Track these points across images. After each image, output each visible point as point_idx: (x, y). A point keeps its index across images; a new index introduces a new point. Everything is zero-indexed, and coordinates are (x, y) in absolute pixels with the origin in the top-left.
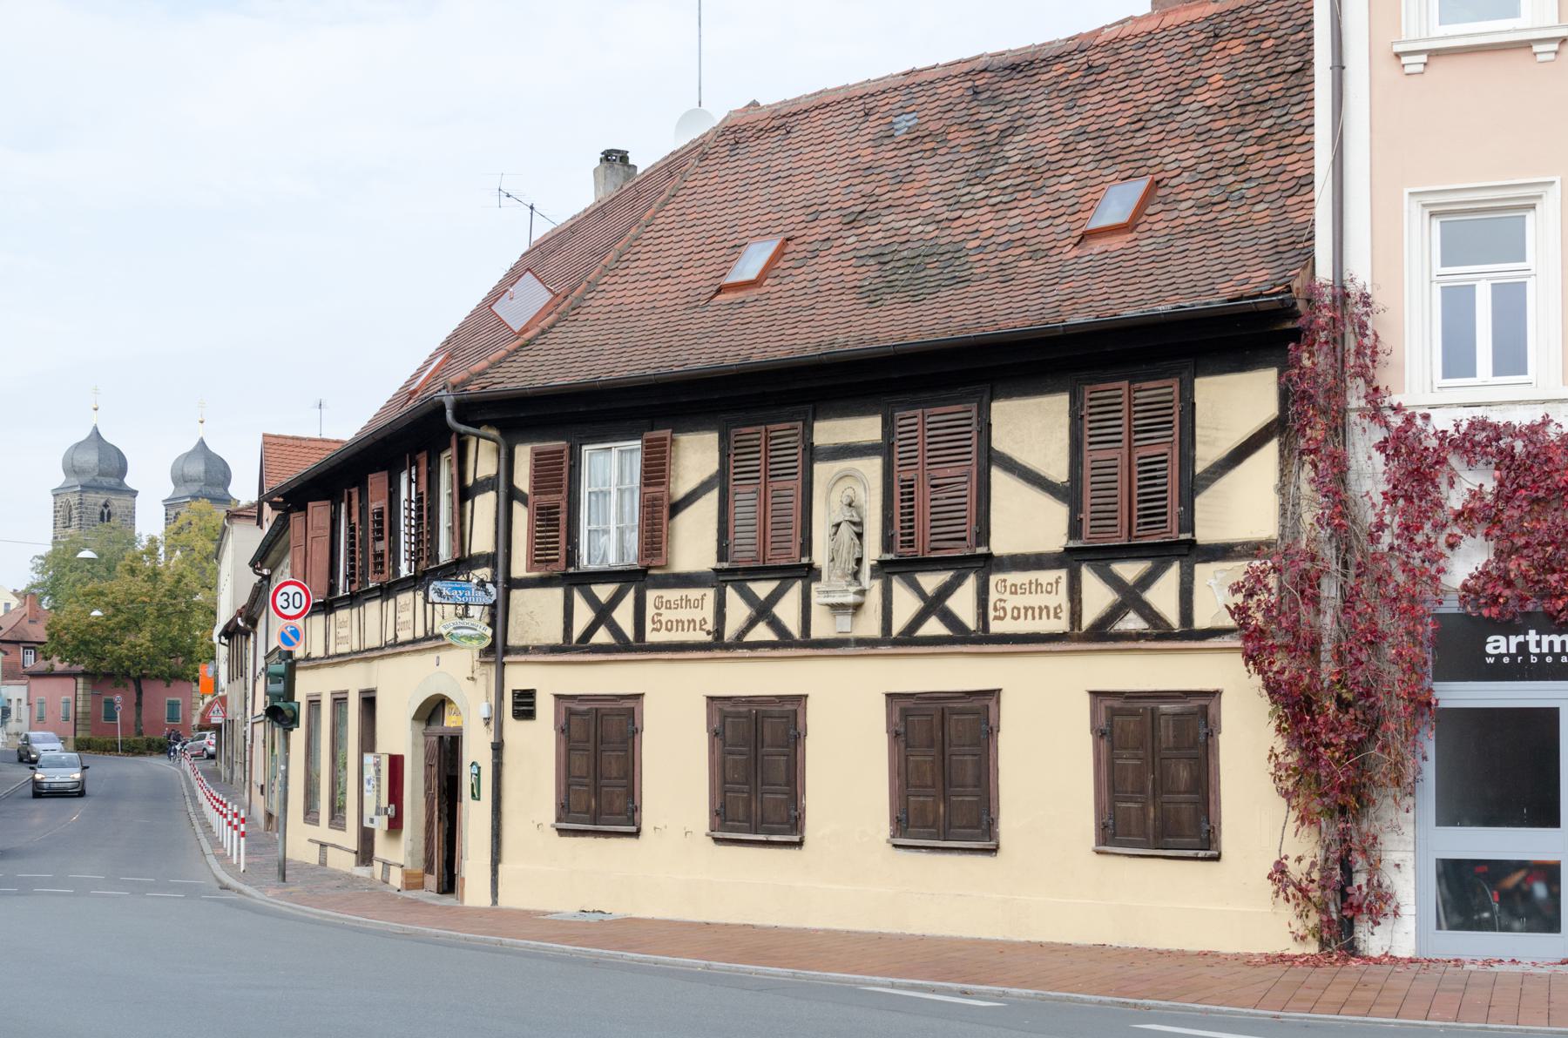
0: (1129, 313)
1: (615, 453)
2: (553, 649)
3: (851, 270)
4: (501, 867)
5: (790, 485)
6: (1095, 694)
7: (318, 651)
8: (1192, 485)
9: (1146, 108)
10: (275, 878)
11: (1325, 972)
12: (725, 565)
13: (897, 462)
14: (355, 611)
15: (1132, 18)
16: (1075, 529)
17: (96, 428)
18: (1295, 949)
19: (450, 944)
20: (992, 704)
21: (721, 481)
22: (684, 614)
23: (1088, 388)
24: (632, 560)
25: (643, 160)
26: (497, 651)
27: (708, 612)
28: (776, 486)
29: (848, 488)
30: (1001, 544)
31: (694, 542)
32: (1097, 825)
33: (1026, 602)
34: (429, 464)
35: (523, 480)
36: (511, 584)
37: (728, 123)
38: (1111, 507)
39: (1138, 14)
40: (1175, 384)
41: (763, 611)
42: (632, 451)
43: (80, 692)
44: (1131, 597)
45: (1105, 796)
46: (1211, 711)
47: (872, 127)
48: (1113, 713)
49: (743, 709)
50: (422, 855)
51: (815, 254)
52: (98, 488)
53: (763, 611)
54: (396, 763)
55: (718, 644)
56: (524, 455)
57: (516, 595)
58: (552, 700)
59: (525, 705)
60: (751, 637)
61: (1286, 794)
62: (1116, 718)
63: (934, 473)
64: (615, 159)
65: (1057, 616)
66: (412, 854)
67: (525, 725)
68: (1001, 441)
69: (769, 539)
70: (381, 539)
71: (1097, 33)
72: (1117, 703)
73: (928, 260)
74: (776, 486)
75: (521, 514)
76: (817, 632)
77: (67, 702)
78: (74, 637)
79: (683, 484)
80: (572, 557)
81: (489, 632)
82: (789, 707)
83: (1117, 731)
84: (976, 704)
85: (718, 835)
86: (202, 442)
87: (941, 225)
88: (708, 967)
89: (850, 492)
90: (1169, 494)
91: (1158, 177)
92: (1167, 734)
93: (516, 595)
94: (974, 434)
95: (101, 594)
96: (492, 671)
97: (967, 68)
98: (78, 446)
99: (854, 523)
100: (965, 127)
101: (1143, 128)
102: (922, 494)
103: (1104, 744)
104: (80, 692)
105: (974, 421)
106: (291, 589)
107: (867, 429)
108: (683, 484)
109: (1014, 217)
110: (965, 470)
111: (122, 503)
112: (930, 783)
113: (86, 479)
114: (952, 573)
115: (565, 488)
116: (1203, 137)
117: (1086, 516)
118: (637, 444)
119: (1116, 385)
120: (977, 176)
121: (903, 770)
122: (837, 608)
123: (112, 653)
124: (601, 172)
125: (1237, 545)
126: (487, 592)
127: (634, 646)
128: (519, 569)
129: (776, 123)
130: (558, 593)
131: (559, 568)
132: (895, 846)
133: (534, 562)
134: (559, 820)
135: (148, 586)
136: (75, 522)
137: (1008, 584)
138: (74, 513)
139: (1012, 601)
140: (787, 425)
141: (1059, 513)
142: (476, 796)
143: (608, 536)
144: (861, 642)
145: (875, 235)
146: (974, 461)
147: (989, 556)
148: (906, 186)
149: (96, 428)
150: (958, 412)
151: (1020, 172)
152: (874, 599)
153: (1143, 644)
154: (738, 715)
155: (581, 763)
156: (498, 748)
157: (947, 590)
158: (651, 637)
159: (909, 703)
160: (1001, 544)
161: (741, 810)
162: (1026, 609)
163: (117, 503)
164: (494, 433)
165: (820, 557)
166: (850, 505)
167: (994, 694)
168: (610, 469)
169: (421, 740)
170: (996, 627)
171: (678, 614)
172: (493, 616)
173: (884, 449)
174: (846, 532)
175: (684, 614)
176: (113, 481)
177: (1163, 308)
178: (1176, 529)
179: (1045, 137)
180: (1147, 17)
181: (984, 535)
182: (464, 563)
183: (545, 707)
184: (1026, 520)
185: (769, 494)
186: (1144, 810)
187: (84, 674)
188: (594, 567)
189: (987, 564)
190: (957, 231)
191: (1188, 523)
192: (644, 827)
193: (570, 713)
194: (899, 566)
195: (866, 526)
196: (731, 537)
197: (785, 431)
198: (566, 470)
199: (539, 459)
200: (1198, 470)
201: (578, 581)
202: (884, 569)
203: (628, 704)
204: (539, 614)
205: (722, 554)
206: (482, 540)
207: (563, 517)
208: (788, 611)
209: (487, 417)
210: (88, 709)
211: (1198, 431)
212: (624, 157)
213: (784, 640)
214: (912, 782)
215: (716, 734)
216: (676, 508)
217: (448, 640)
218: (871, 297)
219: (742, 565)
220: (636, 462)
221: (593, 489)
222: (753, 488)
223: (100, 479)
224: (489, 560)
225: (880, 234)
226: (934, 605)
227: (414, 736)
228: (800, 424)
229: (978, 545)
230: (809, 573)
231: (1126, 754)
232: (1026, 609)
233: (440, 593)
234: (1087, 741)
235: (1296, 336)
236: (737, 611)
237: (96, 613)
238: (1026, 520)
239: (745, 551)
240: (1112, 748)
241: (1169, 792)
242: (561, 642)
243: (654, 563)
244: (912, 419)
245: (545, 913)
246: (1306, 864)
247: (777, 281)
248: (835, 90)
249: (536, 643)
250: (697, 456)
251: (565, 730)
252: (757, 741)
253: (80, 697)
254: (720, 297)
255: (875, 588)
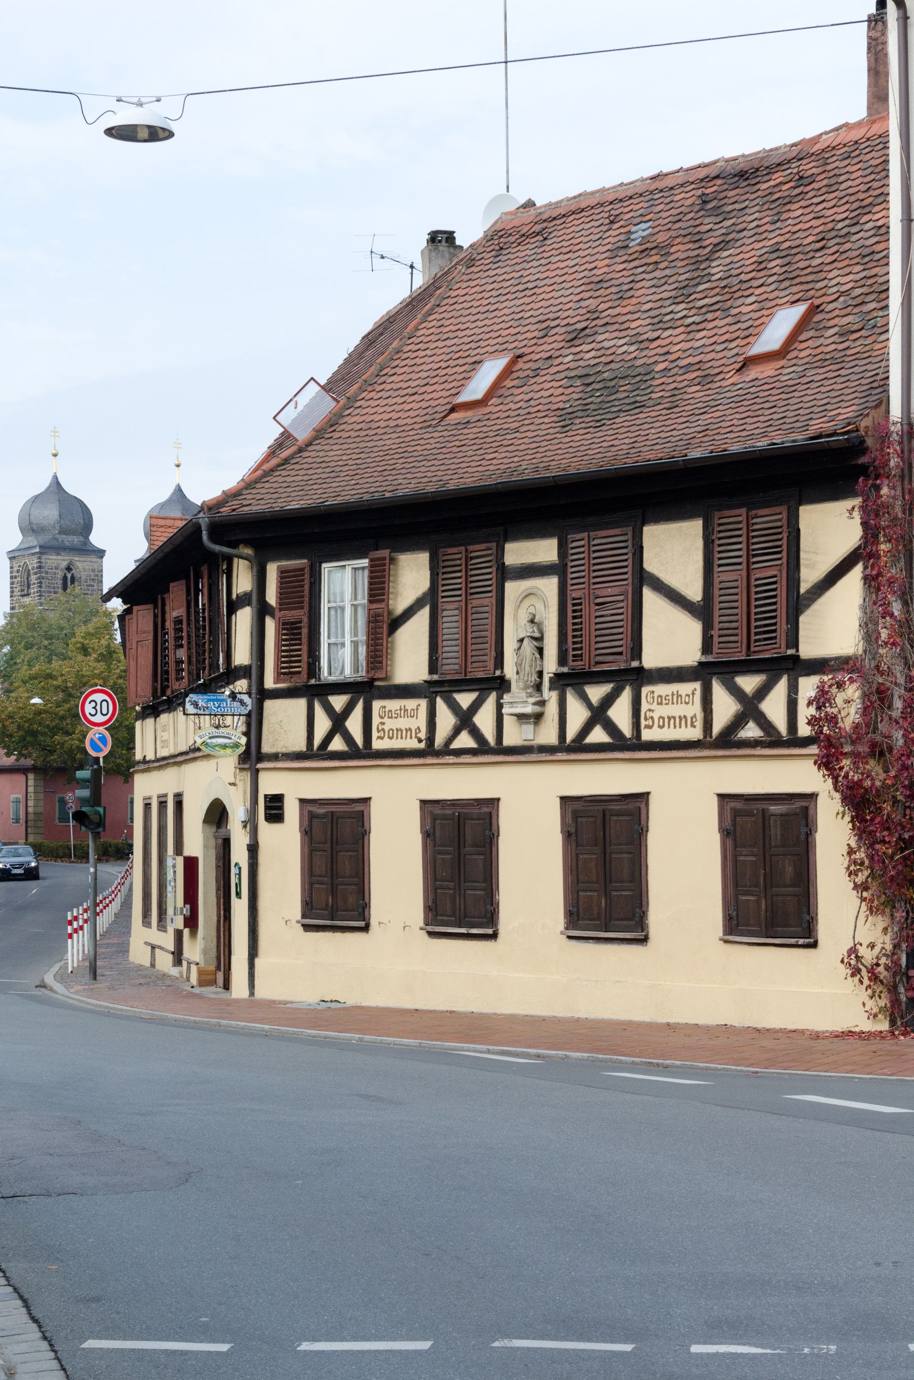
0: (735, 448)
1: (349, 570)
2: (298, 756)
3: (560, 390)
4: (257, 961)
5: (486, 601)
6: (722, 797)
7: (150, 756)
8: (798, 604)
9: (830, 226)
10: (87, 977)
11: (888, 1044)
12: (435, 677)
13: (570, 582)
14: (171, 714)
15: (846, 125)
16: (707, 647)
17: (55, 478)
18: (867, 1026)
19: (109, 1014)
20: (643, 806)
21: (431, 598)
22: (403, 723)
23: (717, 514)
24: (362, 674)
25: (468, 236)
26: (253, 757)
27: (421, 721)
28: (475, 603)
29: (531, 608)
30: (651, 659)
31: (410, 660)
32: (425, 907)
33: (672, 711)
34: (210, 577)
35: (272, 598)
36: (262, 695)
37: (498, 227)
38: (734, 625)
39: (852, 120)
40: (783, 509)
41: (465, 720)
42: (363, 568)
43: (31, 789)
44: (750, 709)
45: (730, 891)
46: (811, 812)
47: (613, 236)
48: (736, 813)
49: (448, 812)
50: (213, 953)
51: (536, 373)
52: (58, 549)
53: (465, 720)
54: (191, 864)
55: (431, 752)
56: (272, 571)
57: (269, 704)
58: (297, 803)
59: (275, 809)
60: (456, 745)
61: (861, 887)
62: (738, 819)
63: (598, 592)
64: (441, 240)
65: (693, 726)
66: (205, 952)
67: (275, 827)
68: (651, 564)
69: (469, 654)
70: (181, 646)
71: (816, 140)
72: (739, 805)
73: (622, 382)
74: (475, 603)
75: (270, 625)
76: (508, 741)
77: (17, 801)
78: (19, 727)
79: (401, 602)
80: (313, 668)
81: (244, 740)
82: (485, 810)
83: (739, 830)
84: (631, 806)
85: (430, 928)
86: (179, 490)
87: (643, 346)
88: (360, 1040)
89: (532, 610)
90: (778, 613)
91: (817, 302)
92: (776, 832)
93: (269, 704)
94: (630, 555)
95: (50, 676)
96: (247, 776)
97: (702, 173)
98: (36, 499)
99: (536, 639)
100: (687, 239)
101: (823, 248)
102: (589, 612)
103: (729, 842)
104: (31, 789)
105: (630, 543)
106: (98, 697)
107: (544, 550)
108: (401, 602)
109: (701, 339)
110: (623, 589)
111: (87, 565)
112: (594, 879)
113: (45, 539)
114: (612, 685)
115: (306, 605)
116: (867, 259)
117: (715, 633)
118: (365, 562)
119: (737, 511)
120: (683, 294)
121: (574, 867)
122: (521, 717)
123: (62, 745)
124: (427, 252)
125: (830, 659)
126: (242, 702)
127: (362, 754)
128: (269, 682)
129: (537, 228)
130: (301, 704)
131: (300, 680)
132: (569, 937)
133: (279, 677)
134: (304, 916)
135: (101, 666)
136: (34, 589)
137: (656, 695)
138: (33, 578)
139: (661, 711)
140: (483, 546)
141: (693, 629)
142: (238, 895)
143: (341, 652)
144: (543, 749)
145: (588, 353)
146: (630, 581)
147: (641, 669)
148: (625, 302)
149: (55, 478)
150: (608, 538)
151: (717, 290)
152: (552, 709)
153: (759, 751)
154: (445, 817)
155: (321, 864)
156: (253, 849)
157: (608, 701)
158: (377, 744)
159: (579, 806)
160: (651, 659)
161: (448, 906)
162: (669, 718)
163: (82, 565)
164: (248, 551)
165: (509, 670)
166: (532, 621)
167: (644, 797)
168: (342, 584)
169: (212, 842)
170: (647, 735)
171: (399, 722)
172: (249, 725)
173: (558, 569)
174: (528, 647)
175: (403, 723)
176: (76, 540)
177: (762, 444)
178: (783, 645)
179: (746, 253)
180: (859, 124)
181: (637, 650)
182: (232, 674)
183: (292, 810)
184: (670, 637)
185: (469, 611)
186: (758, 902)
187: (34, 769)
188: (333, 679)
189: (639, 677)
190: (655, 349)
191: (794, 641)
192: (374, 922)
193: (312, 816)
194: (570, 680)
195: (546, 641)
196: (440, 652)
197: (481, 550)
198: (307, 587)
199: (283, 574)
200: (802, 590)
201: (316, 691)
202: (561, 682)
203: (359, 807)
204: (287, 723)
205: (433, 667)
206: (242, 655)
207: (305, 631)
208: (485, 720)
209: (240, 537)
210: (41, 810)
211: (802, 555)
212: (449, 237)
213: (482, 748)
214: (438, 877)
215: (427, 835)
216: (396, 623)
217: (206, 750)
218: (566, 419)
219: (449, 677)
220: (364, 580)
221: (332, 605)
222: (456, 605)
223: (62, 537)
224: (245, 672)
225: (593, 354)
226: (599, 715)
227: (206, 839)
228: (494, 545)
229: (633, 659)
230: (501, 685)
231: (745, 851)
232: (669, 718)
233: (196, 705)
234: (715, 838)
235: (863, 470)
236: (446, 720)
237: (36, 700)
238: (670, 637)
239: (451, 666)
240: (736, 846)
241: (778, 886)
242: (304, 749)
243: (377, 676)
244: (579, 541)
245: (286, 1003)
246: (877, 949)
247: (500, 401)
248: (593, 193)
249: (284, 750)
250: (412, 575)
251: (307, 832)
252: (459, 841)
253: (31, 795)
254: (453, 416)
255: (552, 697)
